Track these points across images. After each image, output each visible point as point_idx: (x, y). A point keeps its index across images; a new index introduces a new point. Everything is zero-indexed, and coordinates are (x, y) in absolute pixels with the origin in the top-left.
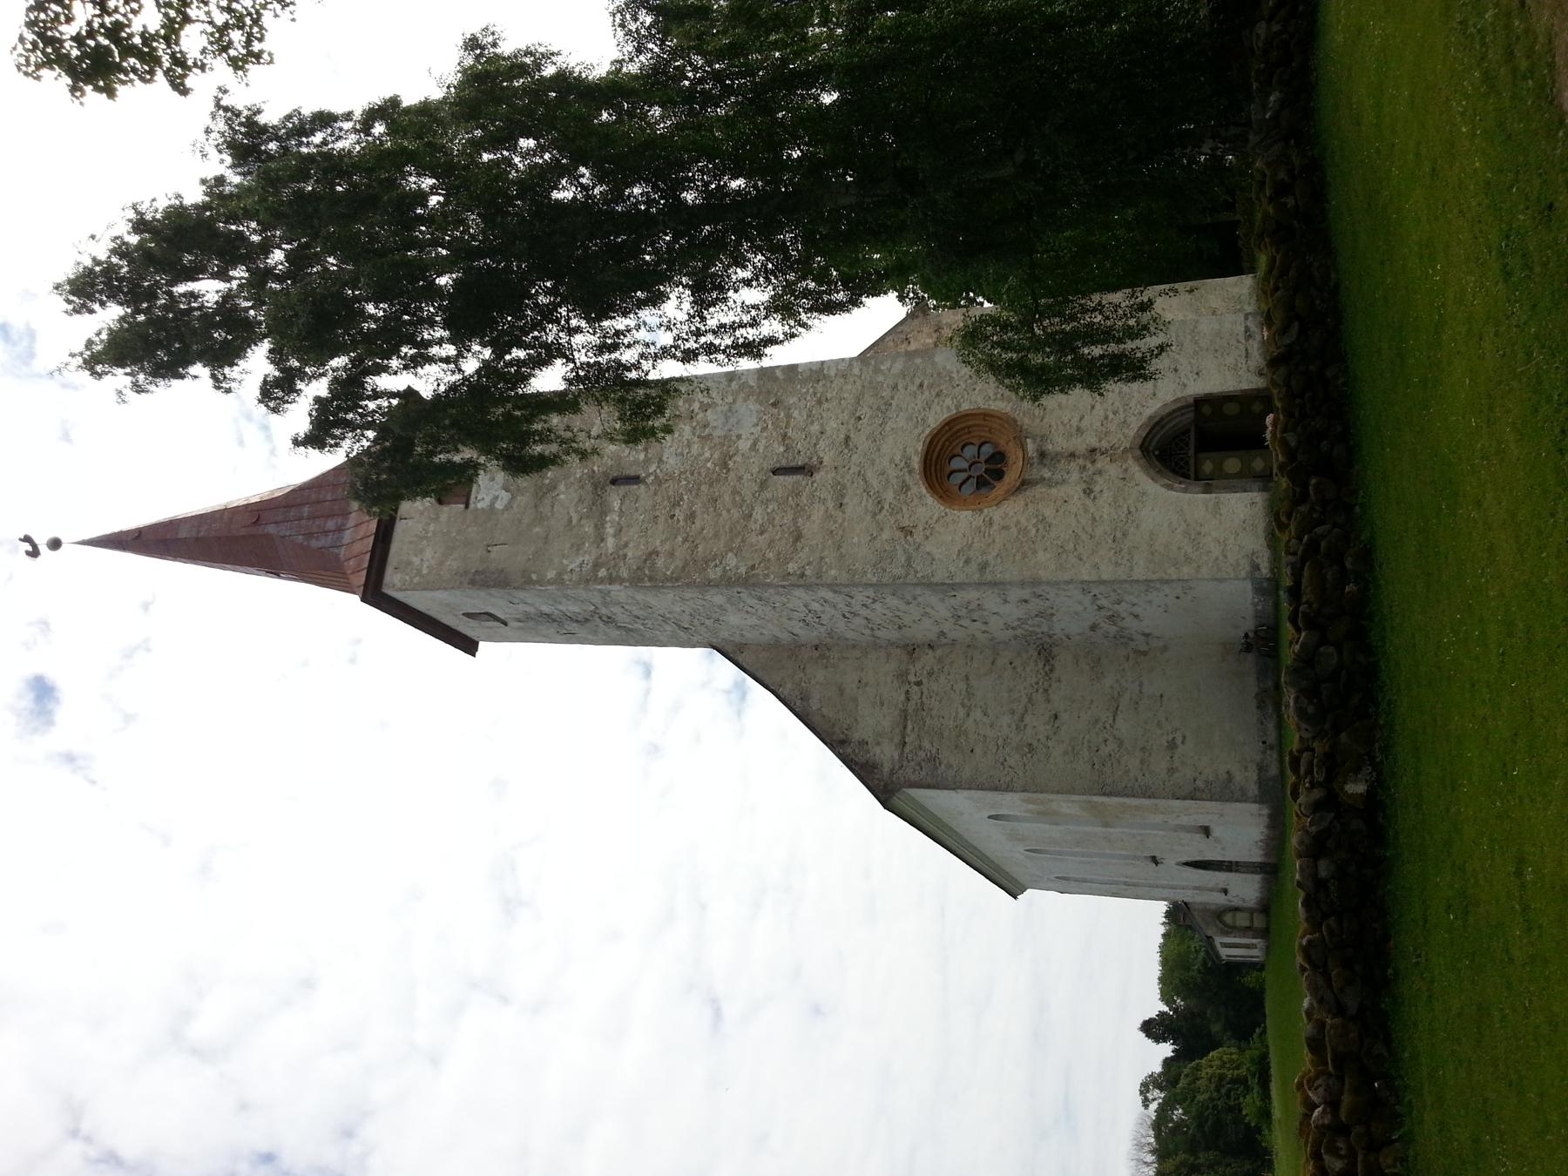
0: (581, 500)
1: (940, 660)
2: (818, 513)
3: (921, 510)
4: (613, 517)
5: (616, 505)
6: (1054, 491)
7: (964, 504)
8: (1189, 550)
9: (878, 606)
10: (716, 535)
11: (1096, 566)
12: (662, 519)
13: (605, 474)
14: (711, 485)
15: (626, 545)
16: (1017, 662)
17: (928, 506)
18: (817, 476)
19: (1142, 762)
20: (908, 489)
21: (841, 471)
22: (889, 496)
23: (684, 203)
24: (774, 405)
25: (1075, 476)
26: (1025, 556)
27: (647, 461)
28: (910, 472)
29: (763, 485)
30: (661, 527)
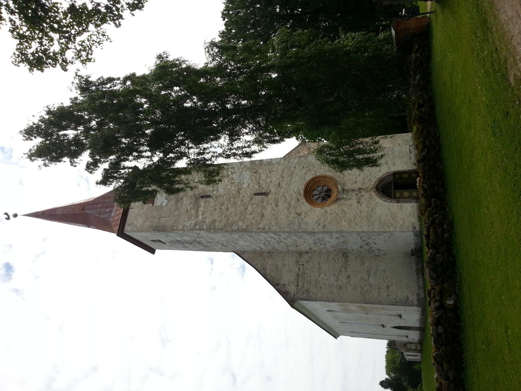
0: (191, 203)
1: (310, 257)
2: (269, 208)
3: (304, 208)
9: (289, 239)
10: (236, 215)
11: (362, 227)
12: (218, 210)
13: (199, 194)
14: (234, 199)
15: (206, 218)
16: (336, 258)
17: (306, 206)
18: (269, 196)
19: (378, 292)
20: (299, 200)
21: (277, 194)
22: (293, 203)
24: (255, 173)
25: (354, 197)
26: (338, 223)
28: (300, 195)
29: (251, 199)
30: (217, 212)
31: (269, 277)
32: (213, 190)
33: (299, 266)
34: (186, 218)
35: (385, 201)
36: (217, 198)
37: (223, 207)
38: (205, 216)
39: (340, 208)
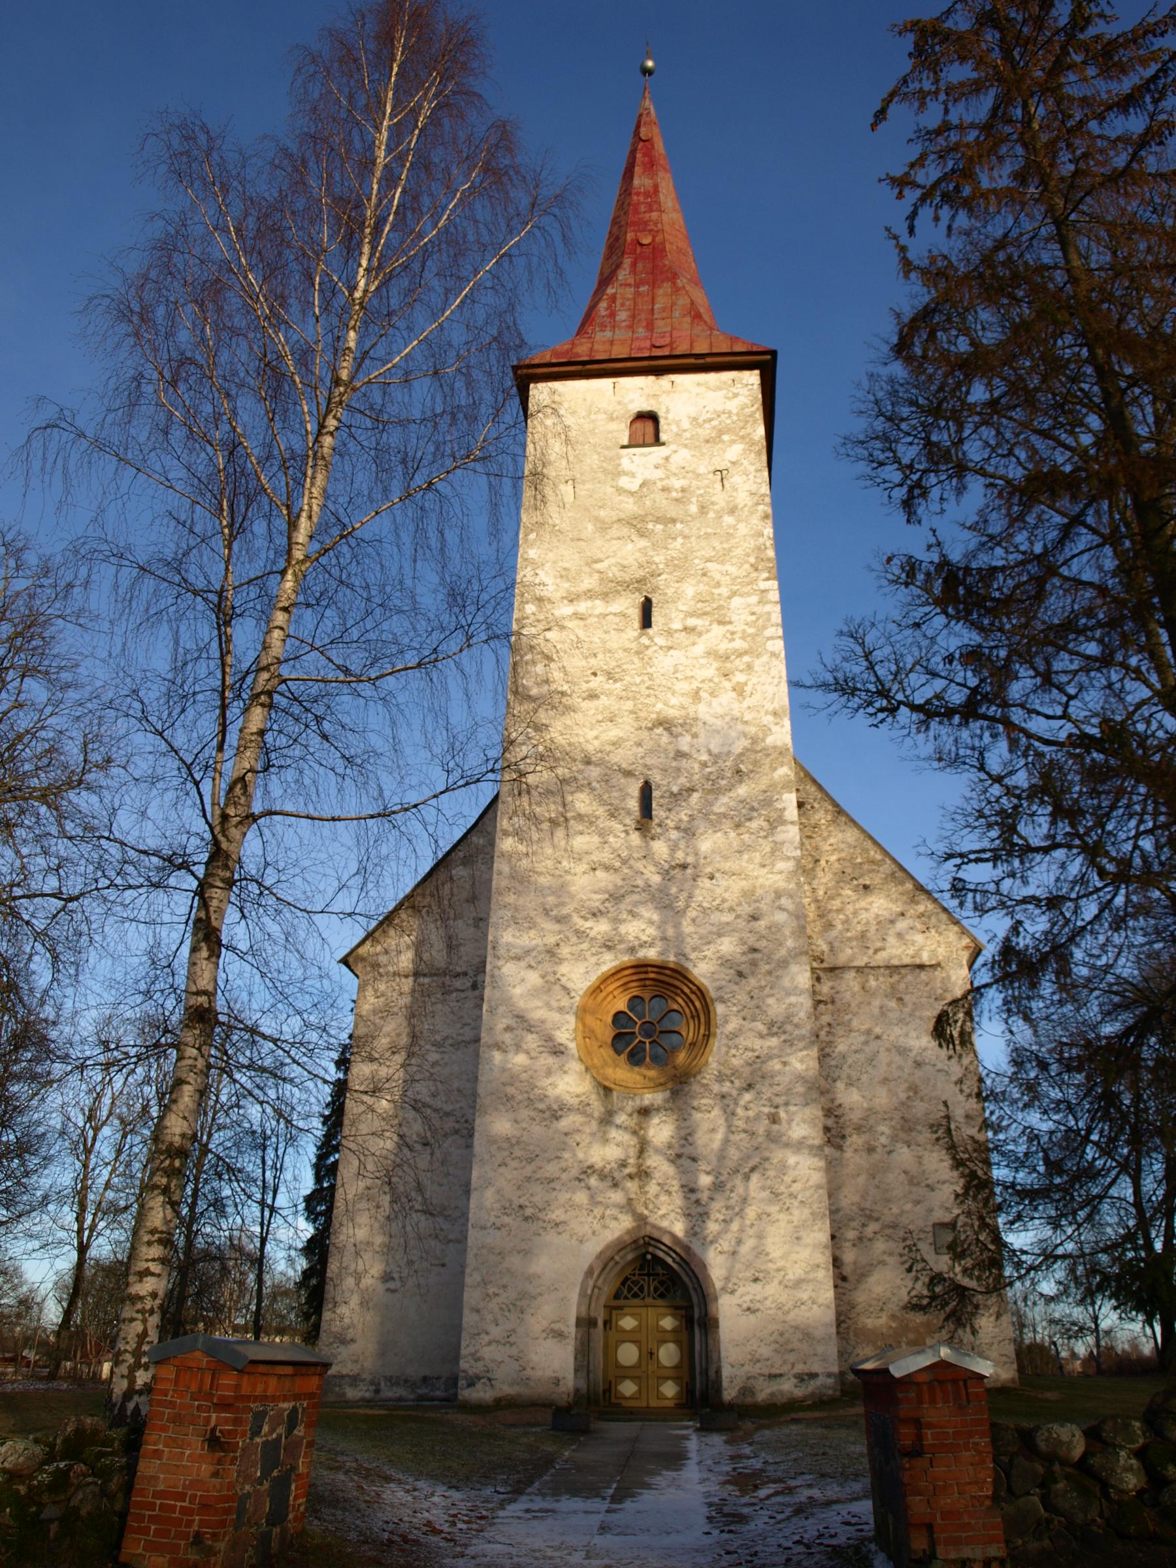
0: (624, 567)
4: (599, 606)
13: (655, 589)
14: (632, 712)
15: (563, 628)
23: (654, 60)
31: (442, 875)
32: (670, 633)
33: (471, 973)
36: (638, 653)
37: (600, 678)
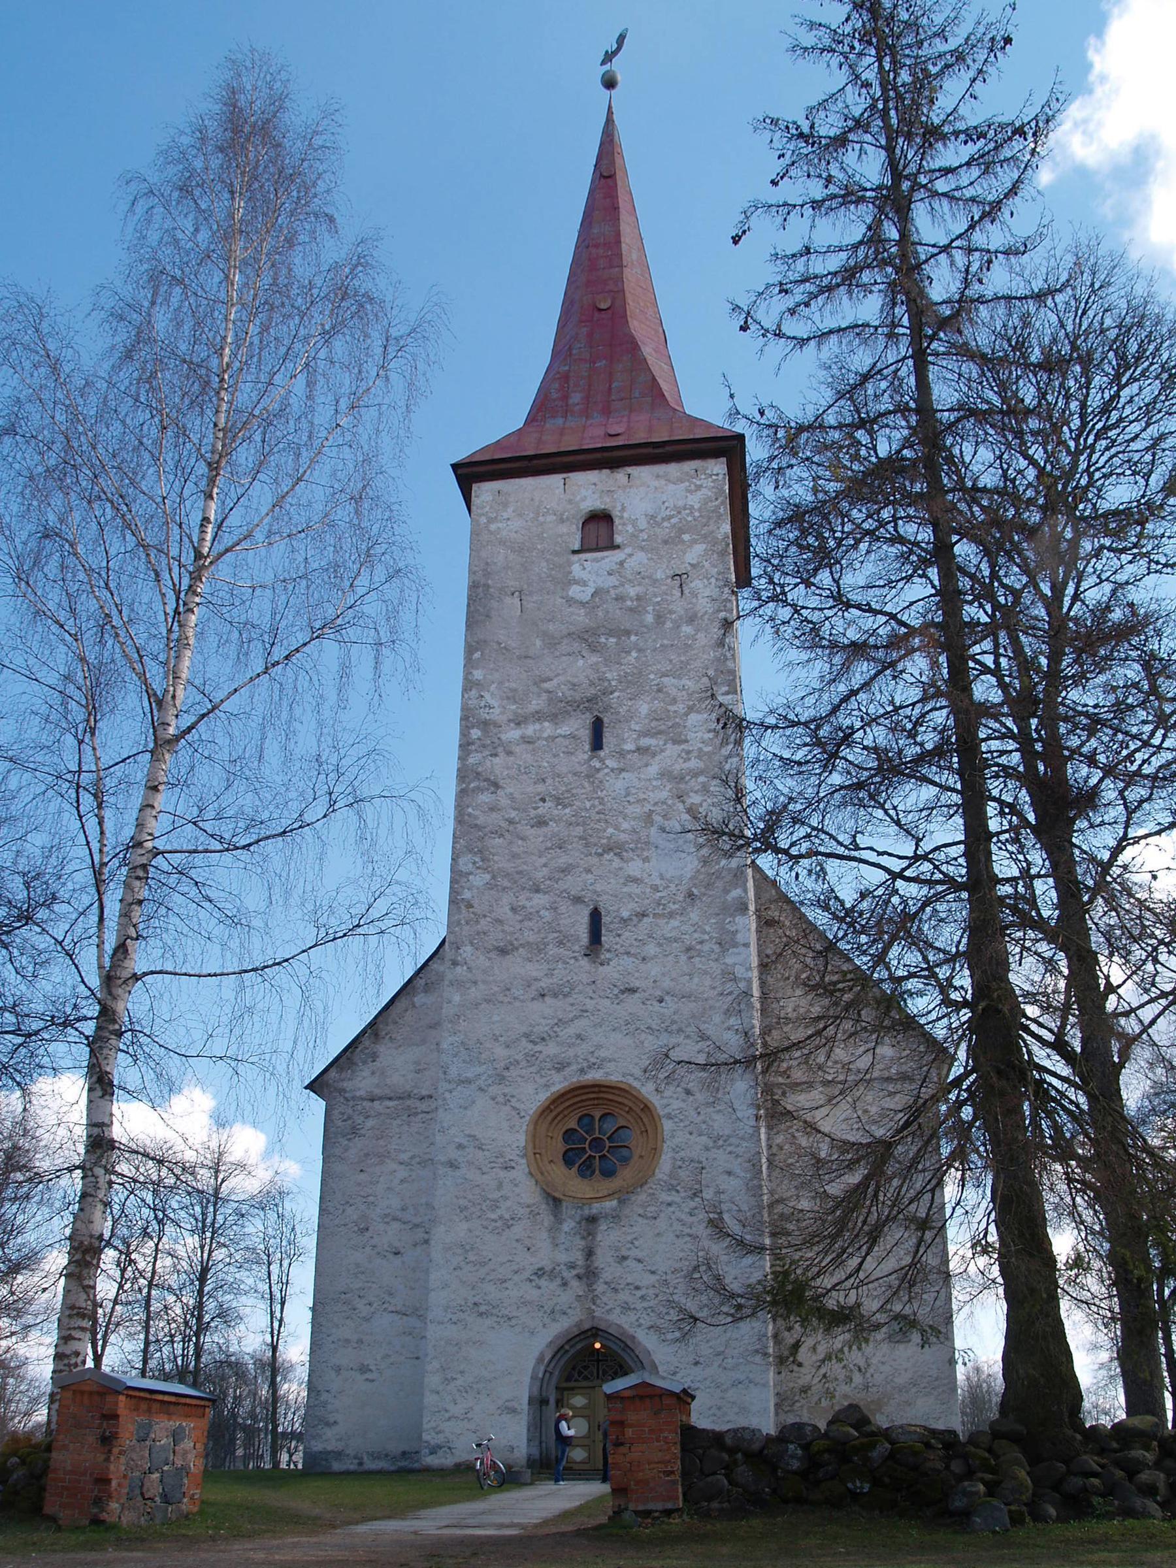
2: (533, 970)
3: (530, 1088)
4: (548, 728)
5: (564, 730)
6: (545, 1235)
7: (534, 1136)
8: (459, 1382)
10: (515, 856)
11: (446, 1286)
12: (541, 788)
13: (607, 708)
14: (581, 838)
15: (509, 753)
17: (534, 1095)
18: (584, 962)
19: (347, 1341)
20: (558, 1070)
21: (589, 990)
22: (551, 1049)
24: (690, 895)
25: (563, 1257)
26: (463, 1209)
27: (622, 754)
28: (582, 1071)
30: (530, 789)
34: (513, 685)
35: (540, 1360)
37: (548, 804)
38: (517, 749)
39: (522, 1211)
